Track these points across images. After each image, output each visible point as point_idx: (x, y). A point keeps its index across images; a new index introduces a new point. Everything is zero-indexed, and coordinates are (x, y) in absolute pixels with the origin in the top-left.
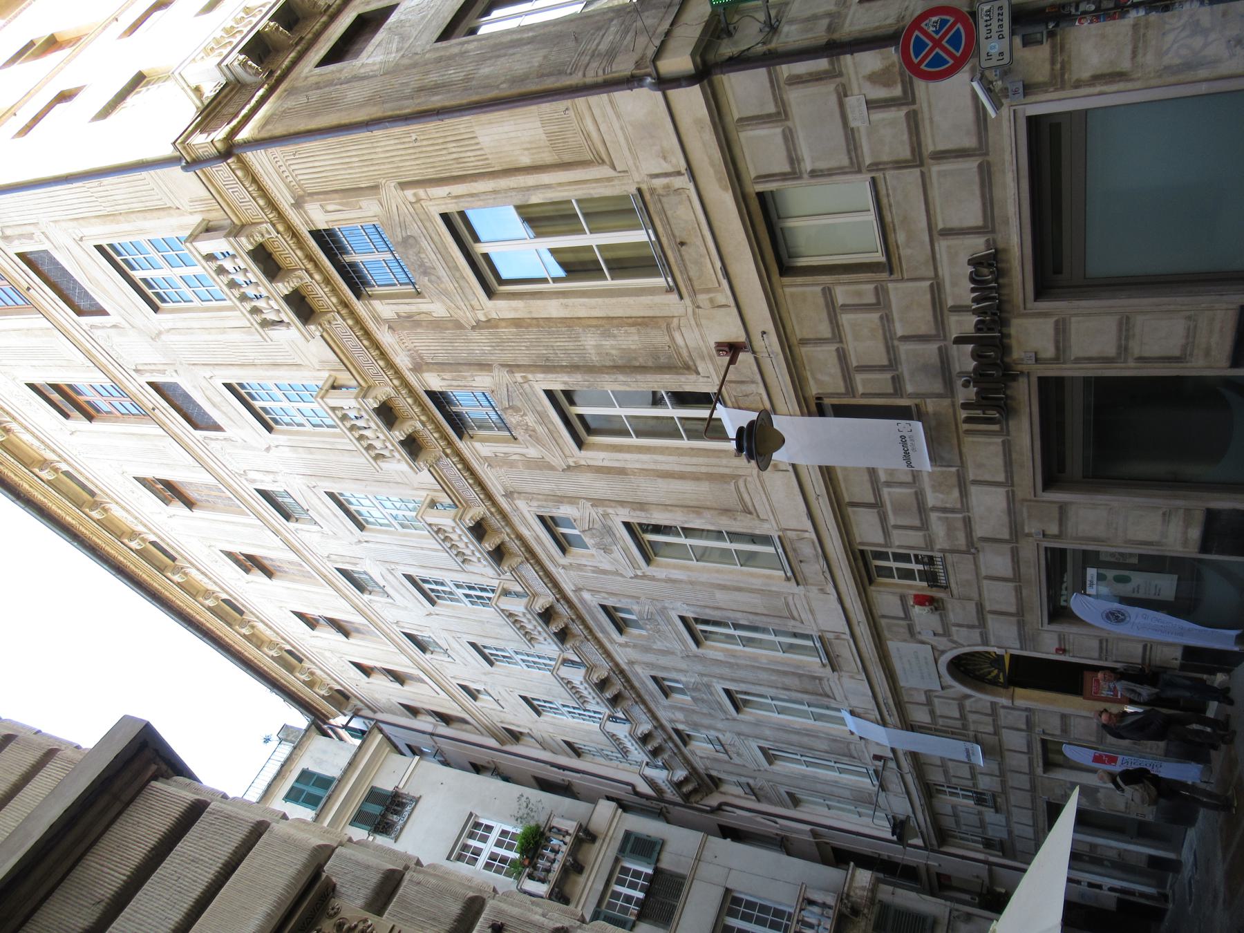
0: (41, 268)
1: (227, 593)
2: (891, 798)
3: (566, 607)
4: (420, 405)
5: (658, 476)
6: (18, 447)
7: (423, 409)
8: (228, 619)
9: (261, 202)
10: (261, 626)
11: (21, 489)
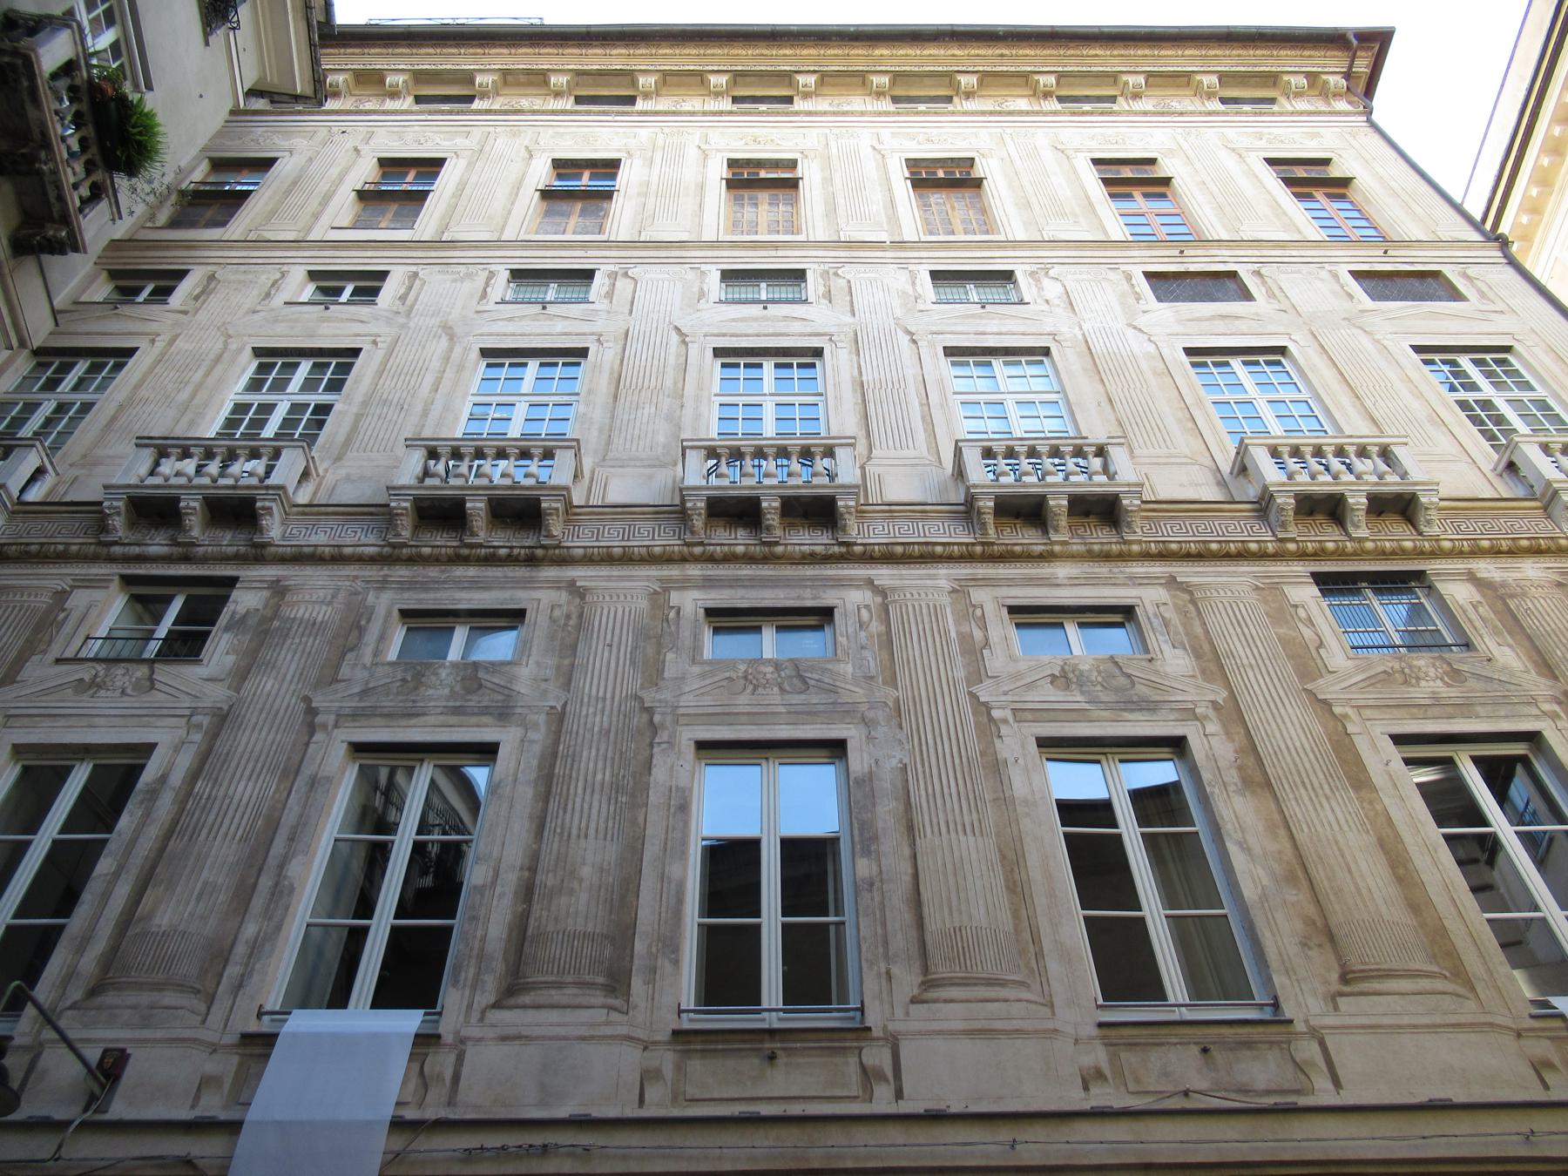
0: (1209, 282)
1: (479, 112)
2: (630, 1060)
3: (818, 549)
4: (1393, 553)
5: (1381, 843)
6: (1008, 86)
7: (1384, 553)
8: (590, 79)
9: (1525, 543)
10: (1022, 104)
11: (956, 44)
